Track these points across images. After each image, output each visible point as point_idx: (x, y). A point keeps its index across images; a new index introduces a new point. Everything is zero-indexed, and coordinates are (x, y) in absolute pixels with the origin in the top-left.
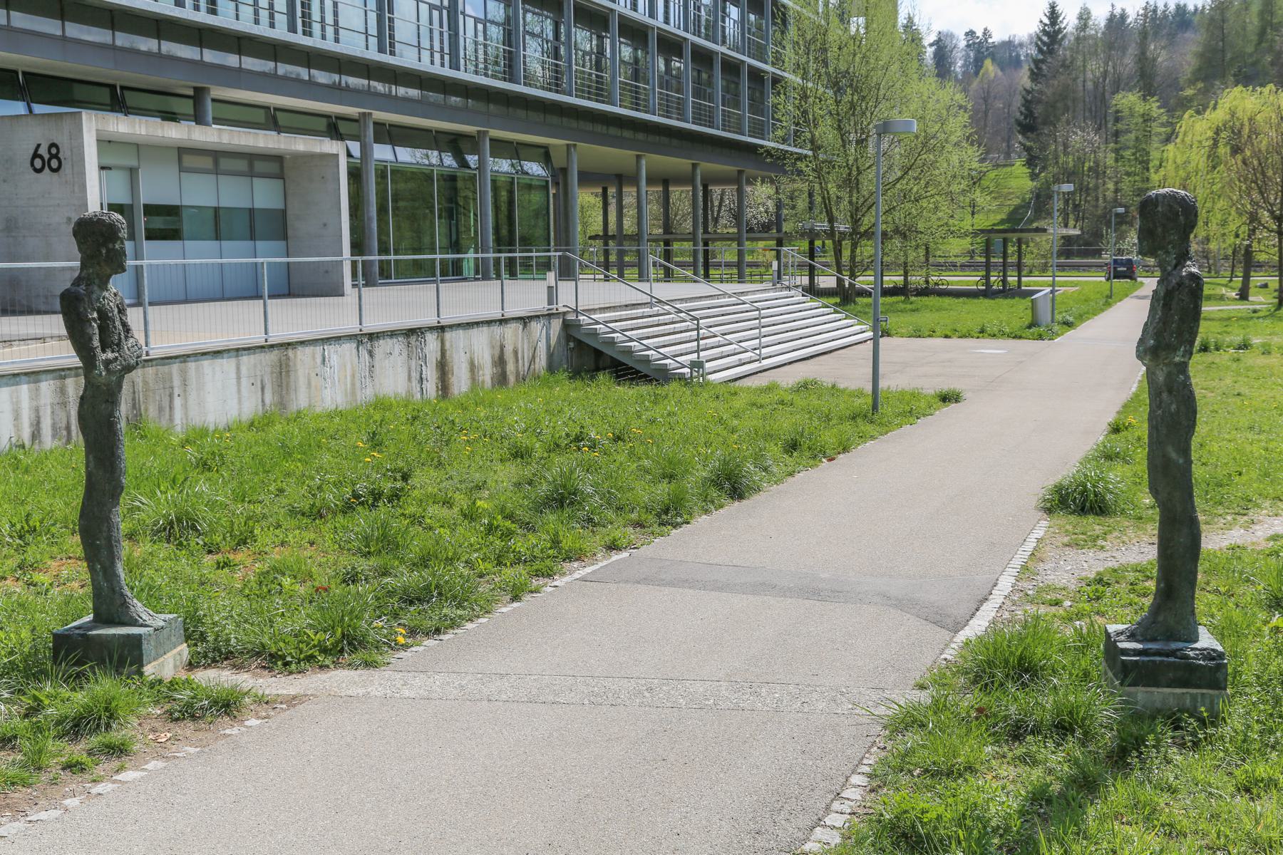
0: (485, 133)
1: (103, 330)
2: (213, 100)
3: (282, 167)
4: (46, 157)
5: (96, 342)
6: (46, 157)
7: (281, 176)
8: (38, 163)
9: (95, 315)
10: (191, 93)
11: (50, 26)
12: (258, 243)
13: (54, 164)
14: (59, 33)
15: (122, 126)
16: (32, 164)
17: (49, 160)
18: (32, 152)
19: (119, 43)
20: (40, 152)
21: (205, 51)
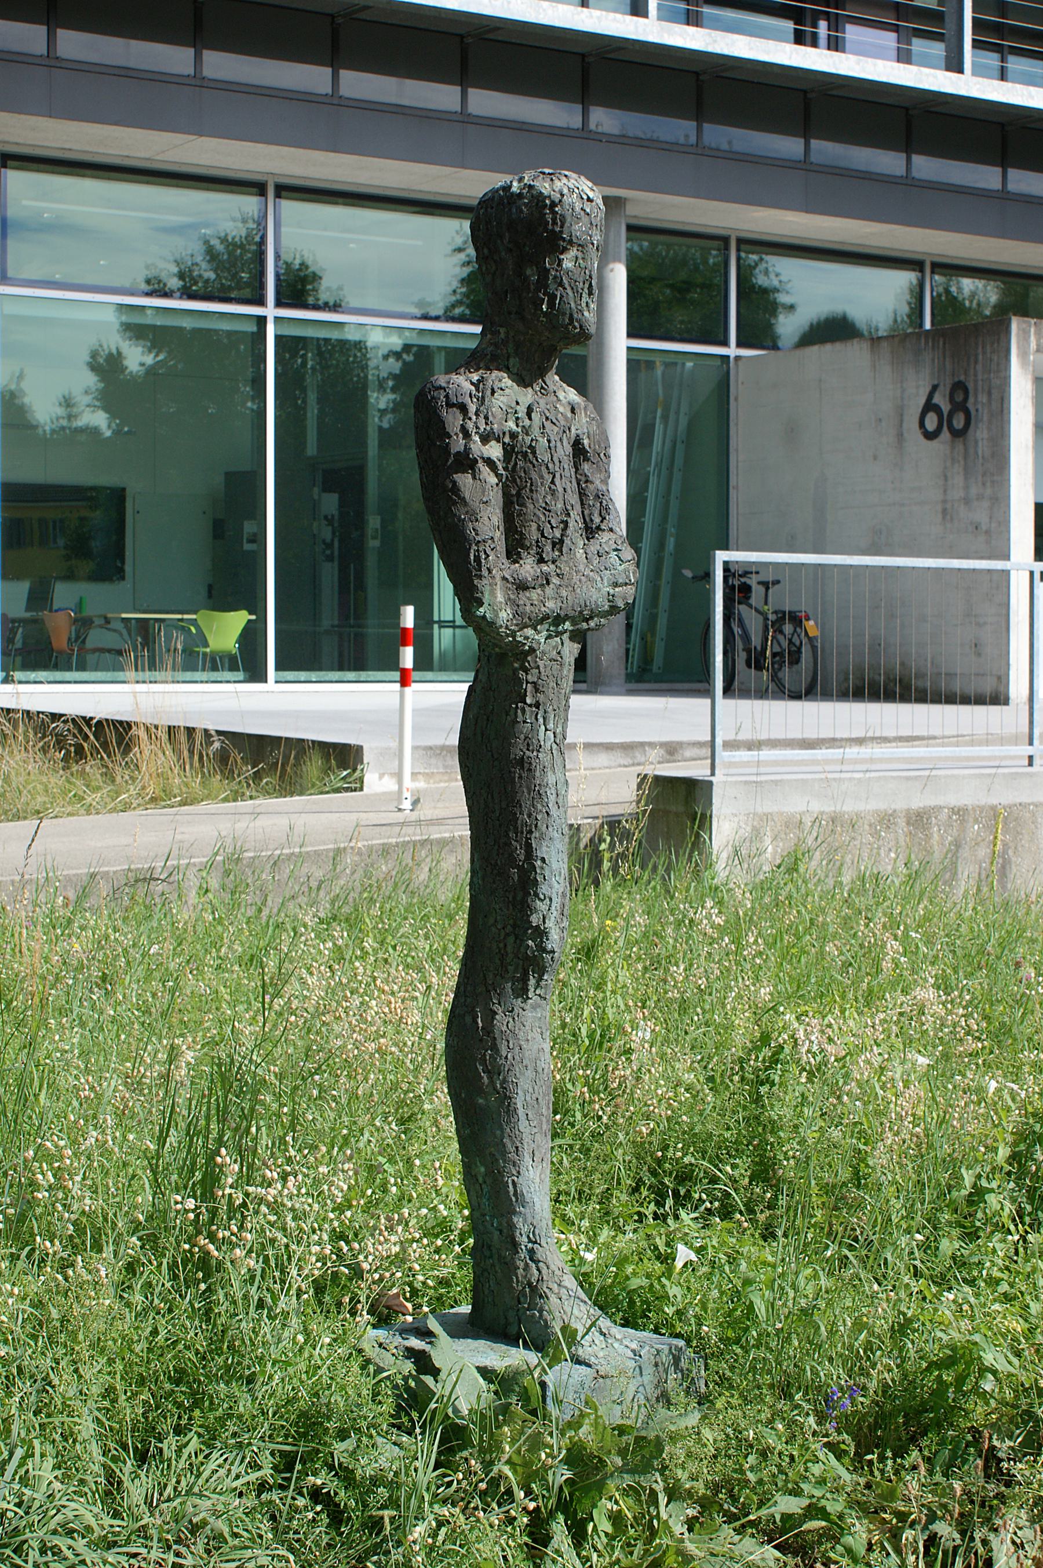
4: (946, 408)
5: (489, 523)
6: (946, 408)
8: (931, 422)
9: (494, 451)
13: (959, 422)
17: (951, 414)
18: (922, 401)
19: (345, 91)
20: (937, 399)
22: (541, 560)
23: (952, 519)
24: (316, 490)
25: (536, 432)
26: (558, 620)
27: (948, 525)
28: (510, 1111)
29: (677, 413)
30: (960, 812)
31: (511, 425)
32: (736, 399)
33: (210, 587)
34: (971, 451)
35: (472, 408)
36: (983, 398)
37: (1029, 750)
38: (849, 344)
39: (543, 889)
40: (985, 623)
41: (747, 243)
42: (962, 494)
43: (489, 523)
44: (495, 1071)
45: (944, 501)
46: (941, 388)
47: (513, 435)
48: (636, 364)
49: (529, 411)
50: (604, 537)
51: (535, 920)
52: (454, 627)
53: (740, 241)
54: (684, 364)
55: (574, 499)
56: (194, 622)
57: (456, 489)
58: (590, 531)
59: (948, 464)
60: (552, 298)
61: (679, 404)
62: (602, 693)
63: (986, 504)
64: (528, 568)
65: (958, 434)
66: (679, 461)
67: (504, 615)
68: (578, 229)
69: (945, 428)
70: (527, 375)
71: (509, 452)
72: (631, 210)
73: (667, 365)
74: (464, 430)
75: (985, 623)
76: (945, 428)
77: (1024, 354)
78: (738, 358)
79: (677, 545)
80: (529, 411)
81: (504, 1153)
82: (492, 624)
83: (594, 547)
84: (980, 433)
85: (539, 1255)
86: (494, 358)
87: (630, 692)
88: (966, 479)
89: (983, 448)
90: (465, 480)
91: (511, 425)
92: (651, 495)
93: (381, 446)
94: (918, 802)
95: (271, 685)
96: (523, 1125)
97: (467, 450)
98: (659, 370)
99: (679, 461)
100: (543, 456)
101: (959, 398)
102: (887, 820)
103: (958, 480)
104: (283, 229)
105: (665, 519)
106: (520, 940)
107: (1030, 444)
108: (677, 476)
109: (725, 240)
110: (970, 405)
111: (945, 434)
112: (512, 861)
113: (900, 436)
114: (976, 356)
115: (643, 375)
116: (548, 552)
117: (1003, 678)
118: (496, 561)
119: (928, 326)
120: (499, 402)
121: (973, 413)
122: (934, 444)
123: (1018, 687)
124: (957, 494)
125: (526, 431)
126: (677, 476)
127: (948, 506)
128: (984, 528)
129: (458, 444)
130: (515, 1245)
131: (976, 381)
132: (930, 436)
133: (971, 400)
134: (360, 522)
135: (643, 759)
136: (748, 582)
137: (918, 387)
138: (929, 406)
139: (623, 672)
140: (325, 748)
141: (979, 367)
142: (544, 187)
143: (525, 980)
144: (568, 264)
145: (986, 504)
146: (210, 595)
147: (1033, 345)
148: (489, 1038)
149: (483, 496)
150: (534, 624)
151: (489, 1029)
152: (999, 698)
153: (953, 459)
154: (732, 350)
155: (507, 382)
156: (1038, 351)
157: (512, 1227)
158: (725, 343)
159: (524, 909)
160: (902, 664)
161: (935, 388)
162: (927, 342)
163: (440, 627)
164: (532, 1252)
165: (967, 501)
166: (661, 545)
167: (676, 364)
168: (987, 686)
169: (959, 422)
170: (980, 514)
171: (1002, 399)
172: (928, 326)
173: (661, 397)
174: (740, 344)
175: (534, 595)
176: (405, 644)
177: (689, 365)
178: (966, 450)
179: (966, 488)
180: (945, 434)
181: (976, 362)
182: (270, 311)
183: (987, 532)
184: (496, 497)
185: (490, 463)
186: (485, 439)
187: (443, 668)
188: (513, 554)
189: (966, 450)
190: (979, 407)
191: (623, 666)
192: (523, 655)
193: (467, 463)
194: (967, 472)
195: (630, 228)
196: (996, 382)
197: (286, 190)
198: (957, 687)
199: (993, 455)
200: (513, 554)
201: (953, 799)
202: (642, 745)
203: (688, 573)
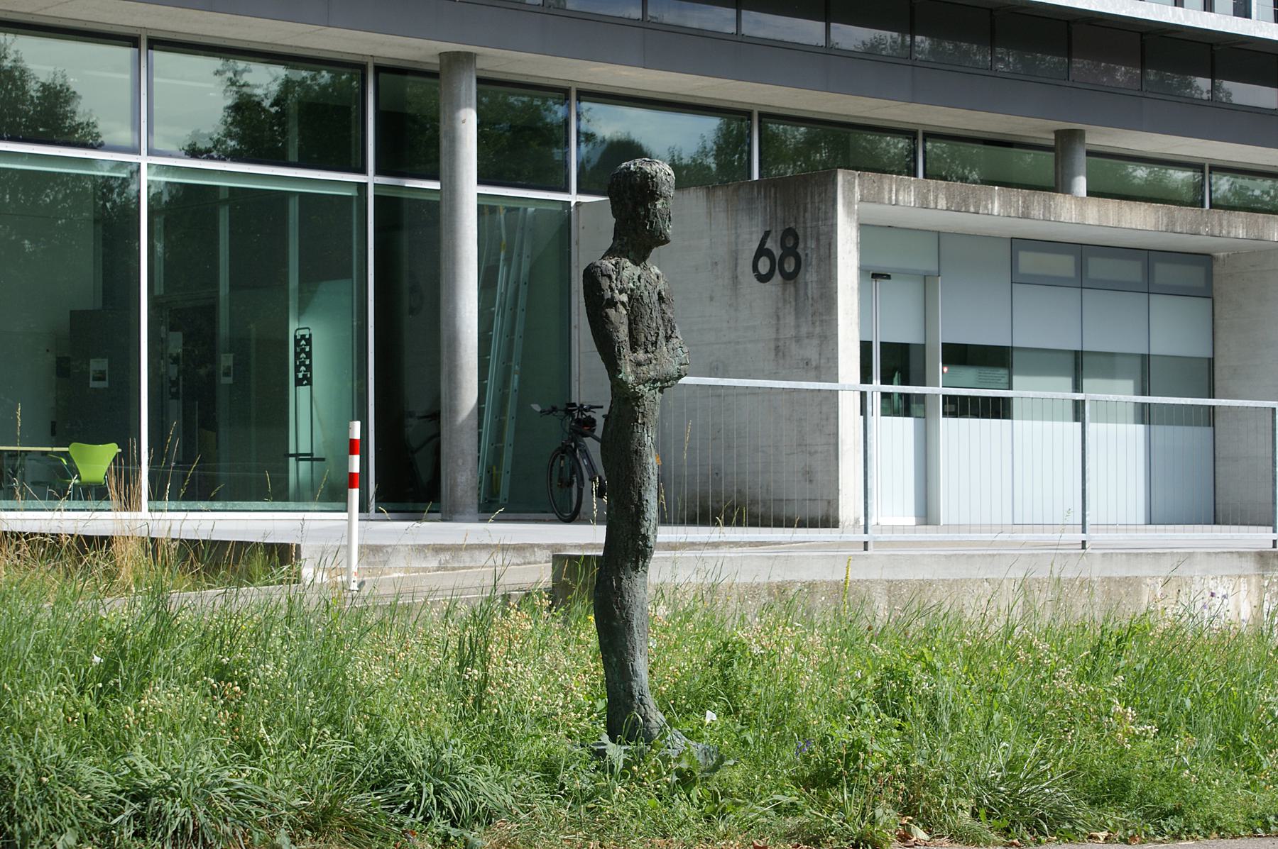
0: (470, 57)
1: (633, 322)
2: (1090, 153)
3: (1209, 276)
4: (777, 252)
5: (623, 334)
6: (777, 252)
7: (1206, 292)
9: (624, 298)
10: (1050, 139)
11: (809, 31)
12: (1157, 429)
13: (790, 266)
14: (731, 29)
15: (905, 199)
16: (755, 267)
17: (782, 259)
18: (756, 246)
19: (746, 30)
20: (769, 245)
21: (747, 15)
22: (647, 352)
23: (784, 355)
24: (163, 328)
25: (642, 288)
26: (655, 381)
27: (781, 362)
28: (630, 628)
29: (520, 255)
30: (811, 586)
31: (631, 285)
32: (577, 243)
33: (54, 424)
34: (802, 292)
35: (614, 277)
36: (812, 244)
37: (865, 538)
38: (686, 192)
39: (647, 515)
40: (816, 452)
41: (587, 95)
42: (793, 332)
43: (623, 334)
44: (623, 608)
45: (777, 340)
46: (773, 233)
47: (632, 290)
48: (486, 209)
49: (639, 278)
50: (674, 341)
51: (643, 531)
52: (312, 460)
53: (379, 69)
54: (526, 209)
55: (660, 322)
56: (66, 455)
57: (607, 316)
58: (668, 338)
59: (780, 305)
60: (652, 223)
61: (521, 248)
62: (456, 521)
63: (815, 342)
64: (641, 355)
65: (789, 277)
66: (522, 302)
67: (631, 378)
68: (664, 189)
69: (777, 271)
70: (639, 259)
71: (630, 298)
72: (480, 63)
73: (509, 210)
74: (610, 287)
75: (816, 452)
76: (777, 271)
77: (849, 204)
78: (578, 204)
79: (521, 381)
80: (639, 278)
81: (627, 650)
82: (625, 383)
83: (670, 346)
84: (810, 276)
85: (645, 701)
86: (621, 252)
87: (481, 521)
88: (797, 318)
89: (813, 290)
90: (611, 312)
91: (631, 285)
92: (495, 335)
93: (232, 287)
94: (776, 579)
95: (144, 514)
96: (636, 635)
97: (613, 297)
98: (502, 215)
99: (522, 302)
100: (646, 301)
101: (790, 243)
102: (753, 591)
103: (790, 320)
104: (155, 80)
105: (509, 358)
106: (635, 541)
107: (856, 286)
108: (521, 316)
109: (362, 67)
110: (800, 250)
111: (777, 277)
112: (632, 501)
113: (735, 278)
114: (806, 204)
115: (487, 217)
116: (650, 348)
117: (833, 503)
118: (626, 351)
119: (756, 177)
120: (626, 274)
121: (803, 257)
122: (767, 286)
123: (849, 507)
124: (789, 332)
125: (638, 288)
126: (521, 316)
127: (781, 344)
128: (814, 364)
129: (608, 294)
130: (632, 697)
131: (805, 228)
132: (763, 279)
133: (801, 245)
134: (210, 357)
135: (532, 559)
136: (593, 415)
137: (751, 233)
138: (762, 251)
139: (476, 501)
140: (269, 548)
141: (808, 215)
142: (648, 169)
143: (637, 562)
144: (659, 206)
145: (815, 342)
146: (53, 433)
147: (857, 196)
148: (619, 592)
149: (619, 317)
150: (644, 382)
151: (619, 587)
152: (829, 521)
153: (785, 301)
154: (573, 198)
155: (629, 264)
156: (861, 200)
157: (631, 687)
158: (566, 190)
159: (638, 525)
160: (739, 491)
161: (767, 234)
162: (759, 192)
163: (298, 460)
164: (641, 700)
165: (798, 339)
166: (505, 382)
167: (518, 209)
168: (819, 513)
169: (790, 266)
170: (811, 352)
171: (830, 244)
172: (756, 177)
173: (504, 242)
174: (579, 191)
175: (645, 368)
176: (352, 452)
177: (531, 210)
178: (797, 291)
179: (798, 326)
180: (777, 277)
181: (805, 211)
182: (370, 179)
183: (817, 368)
184: (625, 320)
185: (623, 303)
186: (620, 292)
187: (299, 498)
188: (633, 349)
189: (797, 291)
190: (809, 252)
191: (476, 496)
192: (637, 398)
193: (612, 303)
194: (798, 313)
195: (480, 81)
196: (823, 229)
197: (158, 43)
198: (785, 512)
199: (822, 296)
200: (633, 349)
201: (805, 576)
202: (532, 546)
203: (537, 408)
